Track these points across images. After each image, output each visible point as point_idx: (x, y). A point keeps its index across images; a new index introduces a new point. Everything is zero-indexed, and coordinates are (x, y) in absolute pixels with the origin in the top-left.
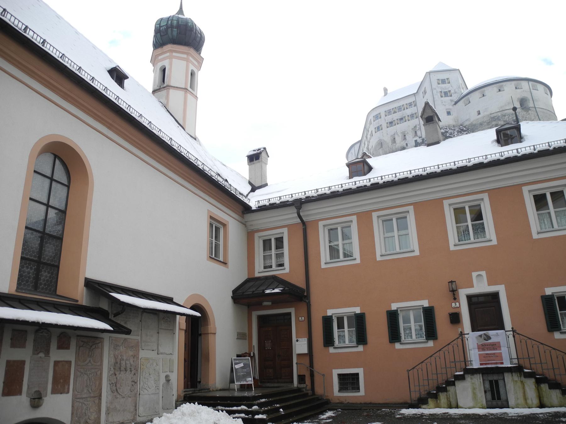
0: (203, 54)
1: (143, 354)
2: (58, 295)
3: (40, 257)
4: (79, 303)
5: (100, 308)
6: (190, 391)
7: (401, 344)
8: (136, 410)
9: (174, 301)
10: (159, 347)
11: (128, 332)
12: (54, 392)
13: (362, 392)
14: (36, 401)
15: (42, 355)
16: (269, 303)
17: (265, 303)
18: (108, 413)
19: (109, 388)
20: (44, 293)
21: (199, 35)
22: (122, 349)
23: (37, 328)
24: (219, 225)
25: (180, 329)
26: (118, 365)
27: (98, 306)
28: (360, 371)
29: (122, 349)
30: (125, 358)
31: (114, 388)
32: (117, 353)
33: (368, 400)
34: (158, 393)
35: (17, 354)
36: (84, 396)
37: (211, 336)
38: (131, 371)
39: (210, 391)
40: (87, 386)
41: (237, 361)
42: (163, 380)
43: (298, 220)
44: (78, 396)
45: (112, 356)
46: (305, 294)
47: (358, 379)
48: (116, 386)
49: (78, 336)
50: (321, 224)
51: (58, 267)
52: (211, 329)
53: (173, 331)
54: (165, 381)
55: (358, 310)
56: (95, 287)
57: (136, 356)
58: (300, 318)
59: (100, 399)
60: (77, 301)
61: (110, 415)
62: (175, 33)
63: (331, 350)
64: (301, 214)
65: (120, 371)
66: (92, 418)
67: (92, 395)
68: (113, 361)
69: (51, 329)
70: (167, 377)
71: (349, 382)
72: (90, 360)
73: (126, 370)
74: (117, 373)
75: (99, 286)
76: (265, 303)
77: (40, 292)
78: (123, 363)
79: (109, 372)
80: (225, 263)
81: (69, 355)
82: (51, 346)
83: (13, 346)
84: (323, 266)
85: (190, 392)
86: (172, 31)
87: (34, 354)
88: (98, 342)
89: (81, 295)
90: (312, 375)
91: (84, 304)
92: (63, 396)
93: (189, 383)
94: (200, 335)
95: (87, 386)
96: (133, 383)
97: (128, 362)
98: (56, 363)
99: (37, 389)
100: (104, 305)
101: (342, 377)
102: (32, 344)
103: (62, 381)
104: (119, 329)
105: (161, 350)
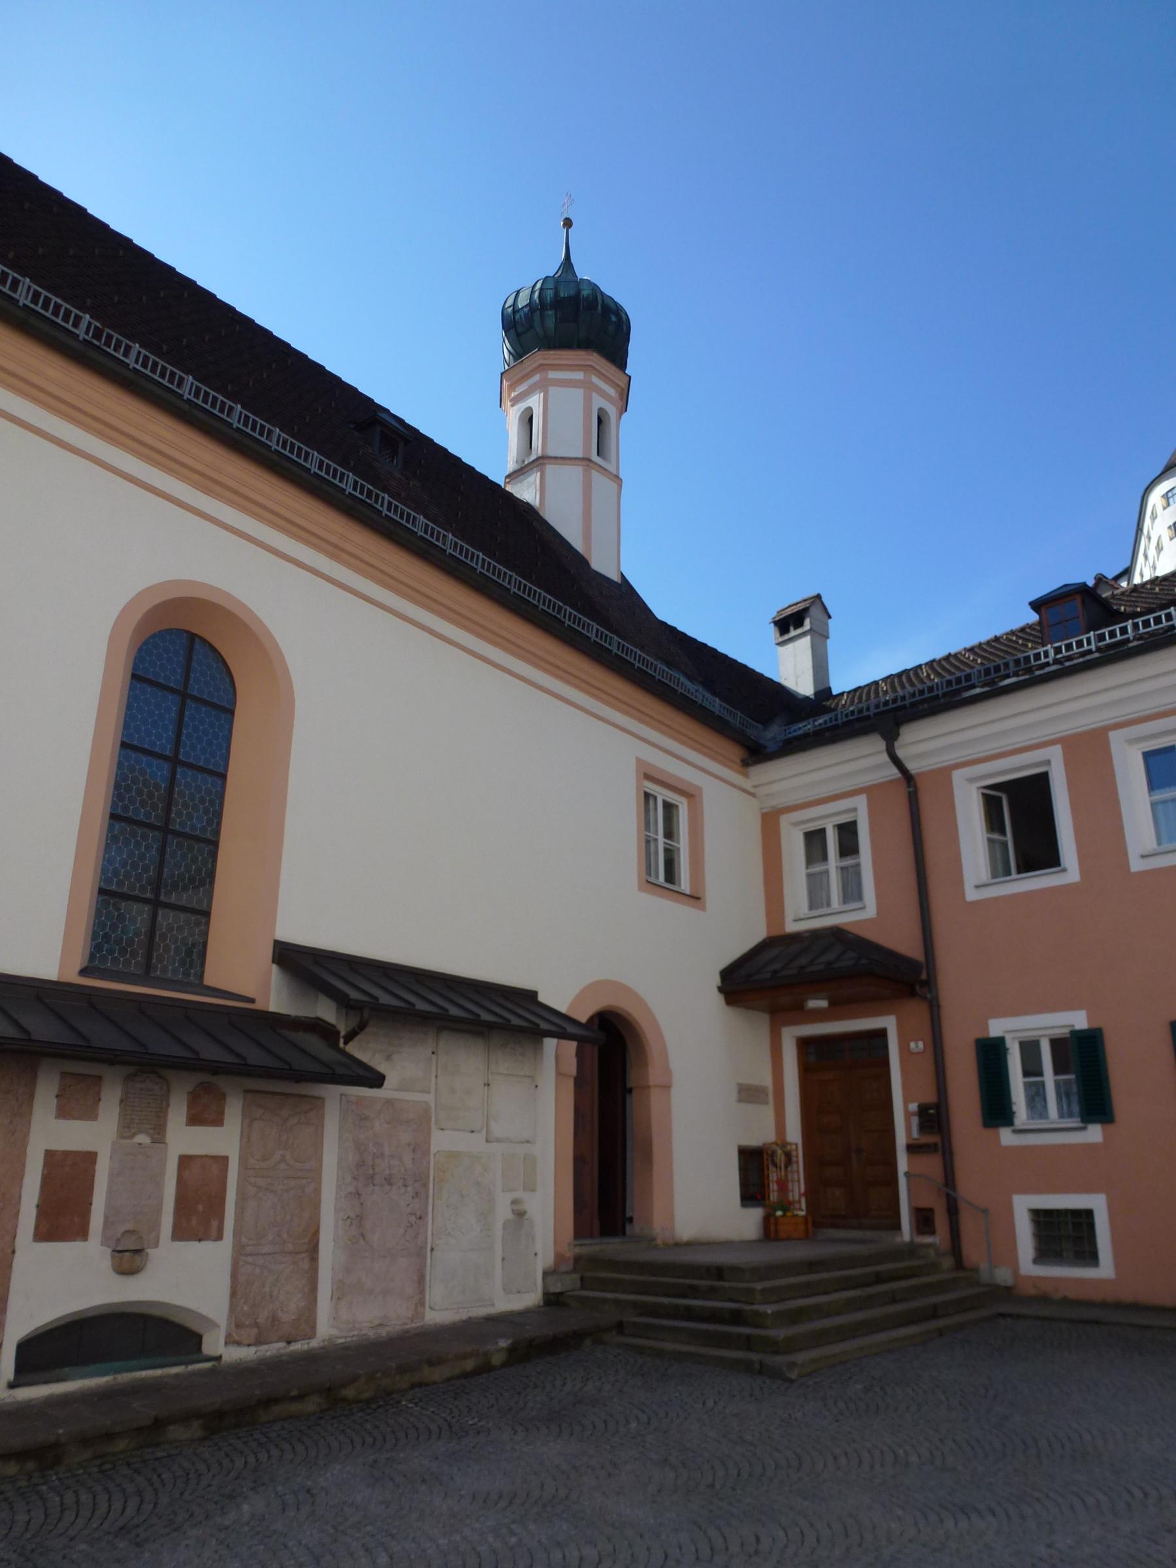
0: (633, 365)
1: (441, 1141)
2: (209, 988)
4: (259, 1006)
5: (318, 1018)
7: (1015, 1132)
9: (542, 998)
11: (376, 1080)
12: (181, 1233)
13: (1105, 1269)
14: (129, 1259)
15: (143, 1139)
16: (823, 1004)
17: (813, 1004)
21: (614, 319)
24: (673, 797)
27: (312, 1015)
28: (1097, 1203)
30: (387, 1151)
33: (1127, 1294)
35: (73, 1135)
36: (265, 1250)
37: (655, 1096)
39: (656, 1247)
42: (503, 1211)
43: (893, 772)
44: (249, 1249)
46: (924, 976)
47: (1091, 1226)
50: (958, 776)
52: (654, 1075)
54: (511, 1216)
55: (1079, 1020)
57: (420, 1149)
58: (912, 1045)
60: (252, 1001)
62: (550, 323)
63: (1006, 1137)
64: (901, 753)
67: (290, 1247)
71: (1065, 1234)
72: (283, 1156)
76: (813, 1004)
80: (695, 898)
84: (971, 895)
86: (542, 317)
90: (953, 1210)
91: (273, 1008)
92: (207, 1246)
94: (630, 1091)
98: (185, 1161)
101: (1043, 1219)
103: (200, 1208)
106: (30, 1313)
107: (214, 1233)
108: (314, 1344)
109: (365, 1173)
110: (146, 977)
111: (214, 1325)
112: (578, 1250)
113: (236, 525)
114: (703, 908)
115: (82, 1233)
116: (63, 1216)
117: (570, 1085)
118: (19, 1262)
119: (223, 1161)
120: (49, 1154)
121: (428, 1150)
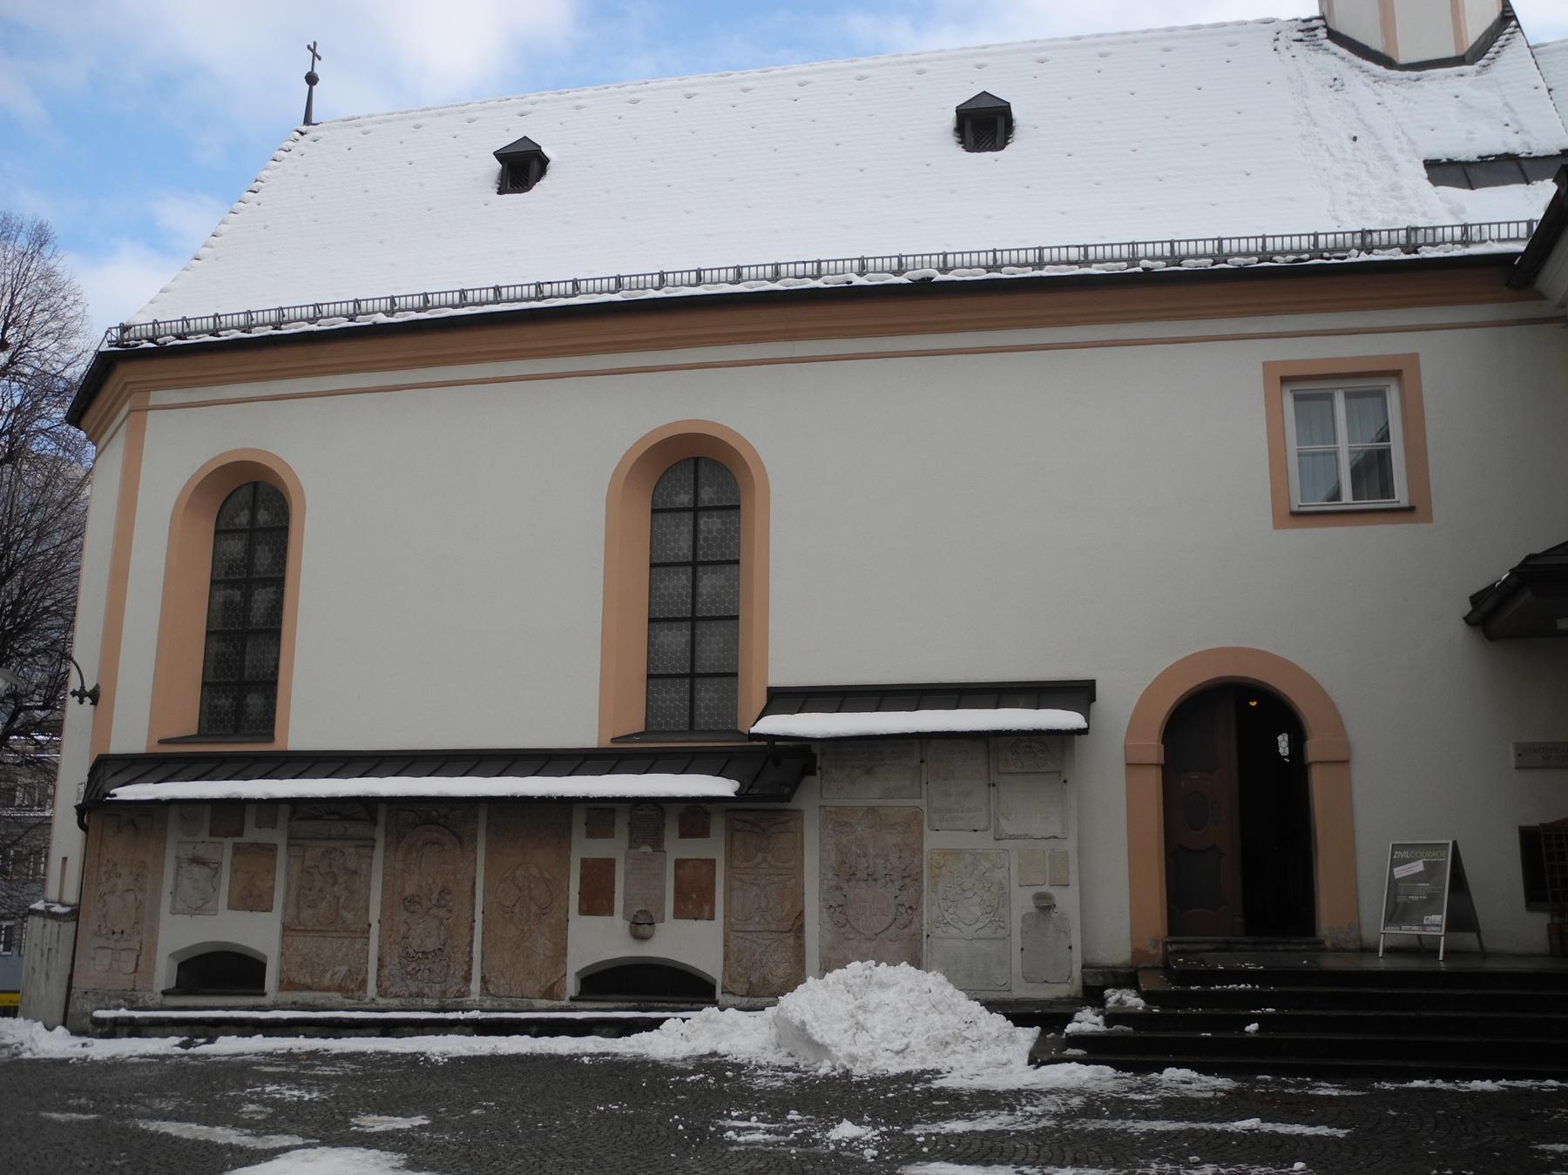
1: (932, 841)
2: (702, 731)
12: (679, 914)
14: (641, 926)
15: (646, 849)
32: (844, 841)
39: (1325, 950)
41: (1406, 854)
42: (1022, 902)
44: (738, 927)
54: (1033, 910)
67: (774, 927)
83: (684, 834)
98: (679, 864)
102: (626, 830)
107: (707, 914)
109: (844, 872)
113: (135, 559)
114: (1428, 518)
115: (610, 911)
116: (596, 900)
117: (1153, 779)
118: (572, 925)
120: (584, 861)
121: (921, 850)
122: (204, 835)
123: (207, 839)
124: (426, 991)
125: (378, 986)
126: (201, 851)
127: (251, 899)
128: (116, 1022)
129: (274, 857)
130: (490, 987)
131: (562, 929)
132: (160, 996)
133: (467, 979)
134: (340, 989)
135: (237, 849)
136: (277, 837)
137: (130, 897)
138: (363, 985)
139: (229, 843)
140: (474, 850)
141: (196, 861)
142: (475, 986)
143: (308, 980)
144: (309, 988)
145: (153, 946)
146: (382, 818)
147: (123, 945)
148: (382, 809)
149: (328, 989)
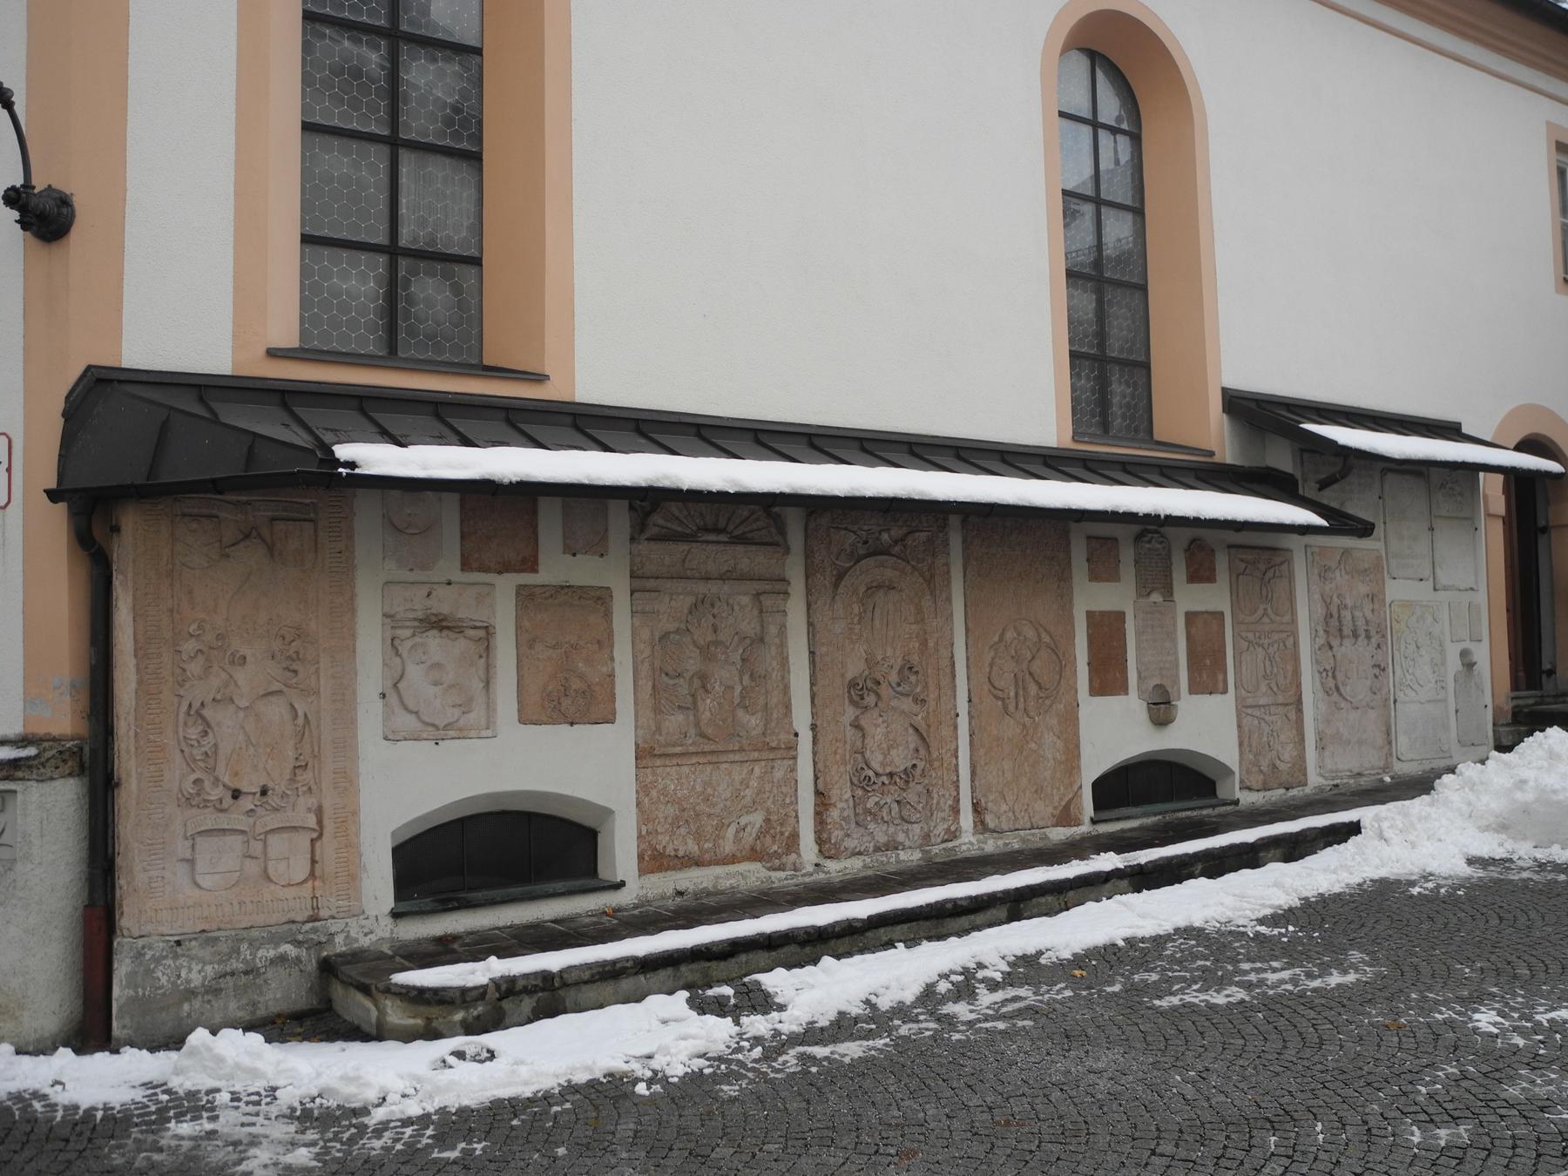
1: (1395, 591)
2: (1159, 443)
3: (1102, 345)
4: (1217, 459)
5: (1268, 468)
6: (1529, 698)
8: (1390, 743)
9: (1465, 430)
10: (1438, 571)
11: (1365, 530)
12: (1195, 688)
14: (1161, 711)
15: (1156, 597)
18: (1321, 747)
19: (1318, 683)
20: (1133, 440)
22: (1340, 578)
23: (1136, 528)
25: (1489, 515)
26: (1334, 623)
29: (1340, 578)
30: (1349, 602)
31: (1331, 683)
34: (1445, 700)
38: (1368, 637)
40: (1265, 677)
42: (1454, 664)
44: (1250, 701)
45: (1317, 596)
48: (1334, 677)
49: (1230, 547)
51: (1146, 366)
53: (1470, 521)
54: (1460, 668)
56: (1254, 413)
57: (1375, 597)
59: (1300, 710)
60: (1212, 454)
61: (1327, 753)
65: (1342, 637)
66: (1286, 756)
67: (1280, 699)
68: (1320, 611)
69: (1168, 530)
70: (1464, 654)
73: (1355, 635)
74: (1335, 643)
75: (1289, 411)
77: (1115, 437)
78: (1347, 615)
79: (1313, 640)
81: (1213, 597)
82: (1175, 575)
83: (1094, 577)
85: (1531, 701)
87: (1139, 595)
88: (1278, 560)
89: (1218, 438)
91: (1229, 460)
92: (1216, 699)
93: (1521, 674)
95: (1265, 677)
96: (1377, 671)
97: (1358, 614)
98: (1191, 617)
99: (1157, 681)
100: (1281, 458)
104: (1343, 523)
105: (1443, 579)
106: (1096, 761)
107: (1221, 685)
108: (1308, 790)
109: (1334, 627)
110: (391, 355)
111: (1227, 771)
112: (1516, 702)
115: (1122, 689)
116: (1108, 679)
118: (1083, 713)
119: (1219, 616)
120: (1090, 614)
122: (448, 566)
123: (457, 575)
124: (901, 837)
125: (820, 841)
126: (444, 602)
127: (569, 700)
128: (508, 988)
129: (608, 615)
130: (990, 821)
131: (1070, 720)
132: (387, 922)
133: (956, 810)
134: (755, 855)
135: (526, 597)
136: (608, 572)
137: (275, 711)
138: (793, 842)
139: (505, 586)
140: (949, 599)
141: (438, 624)
142: (967, 819)
143: (692, 847)
144: (699, 863)
145: (350, 817)
146: (796, 539)
147: (272, 821)
148: (955, 521)
149: (732, 859)
